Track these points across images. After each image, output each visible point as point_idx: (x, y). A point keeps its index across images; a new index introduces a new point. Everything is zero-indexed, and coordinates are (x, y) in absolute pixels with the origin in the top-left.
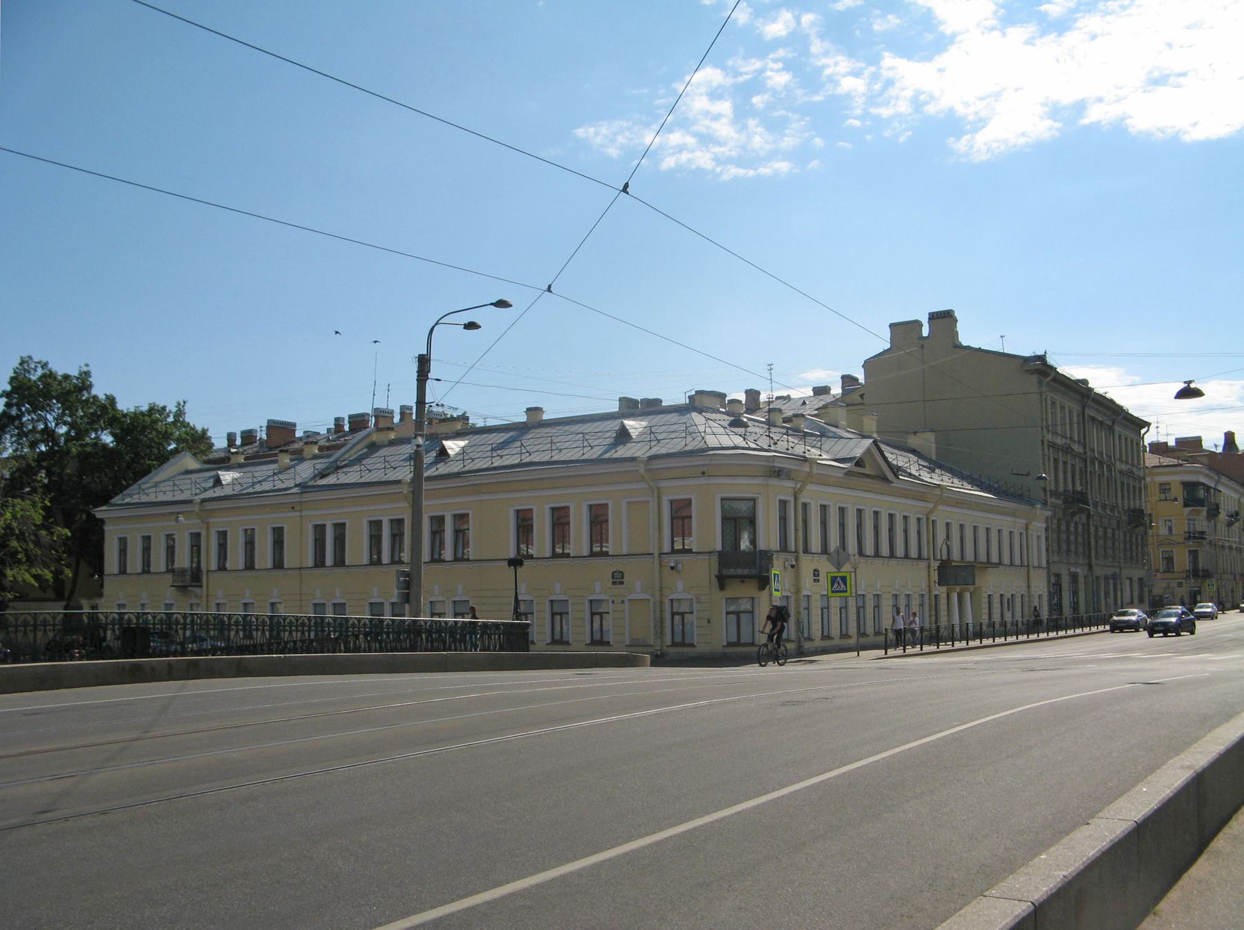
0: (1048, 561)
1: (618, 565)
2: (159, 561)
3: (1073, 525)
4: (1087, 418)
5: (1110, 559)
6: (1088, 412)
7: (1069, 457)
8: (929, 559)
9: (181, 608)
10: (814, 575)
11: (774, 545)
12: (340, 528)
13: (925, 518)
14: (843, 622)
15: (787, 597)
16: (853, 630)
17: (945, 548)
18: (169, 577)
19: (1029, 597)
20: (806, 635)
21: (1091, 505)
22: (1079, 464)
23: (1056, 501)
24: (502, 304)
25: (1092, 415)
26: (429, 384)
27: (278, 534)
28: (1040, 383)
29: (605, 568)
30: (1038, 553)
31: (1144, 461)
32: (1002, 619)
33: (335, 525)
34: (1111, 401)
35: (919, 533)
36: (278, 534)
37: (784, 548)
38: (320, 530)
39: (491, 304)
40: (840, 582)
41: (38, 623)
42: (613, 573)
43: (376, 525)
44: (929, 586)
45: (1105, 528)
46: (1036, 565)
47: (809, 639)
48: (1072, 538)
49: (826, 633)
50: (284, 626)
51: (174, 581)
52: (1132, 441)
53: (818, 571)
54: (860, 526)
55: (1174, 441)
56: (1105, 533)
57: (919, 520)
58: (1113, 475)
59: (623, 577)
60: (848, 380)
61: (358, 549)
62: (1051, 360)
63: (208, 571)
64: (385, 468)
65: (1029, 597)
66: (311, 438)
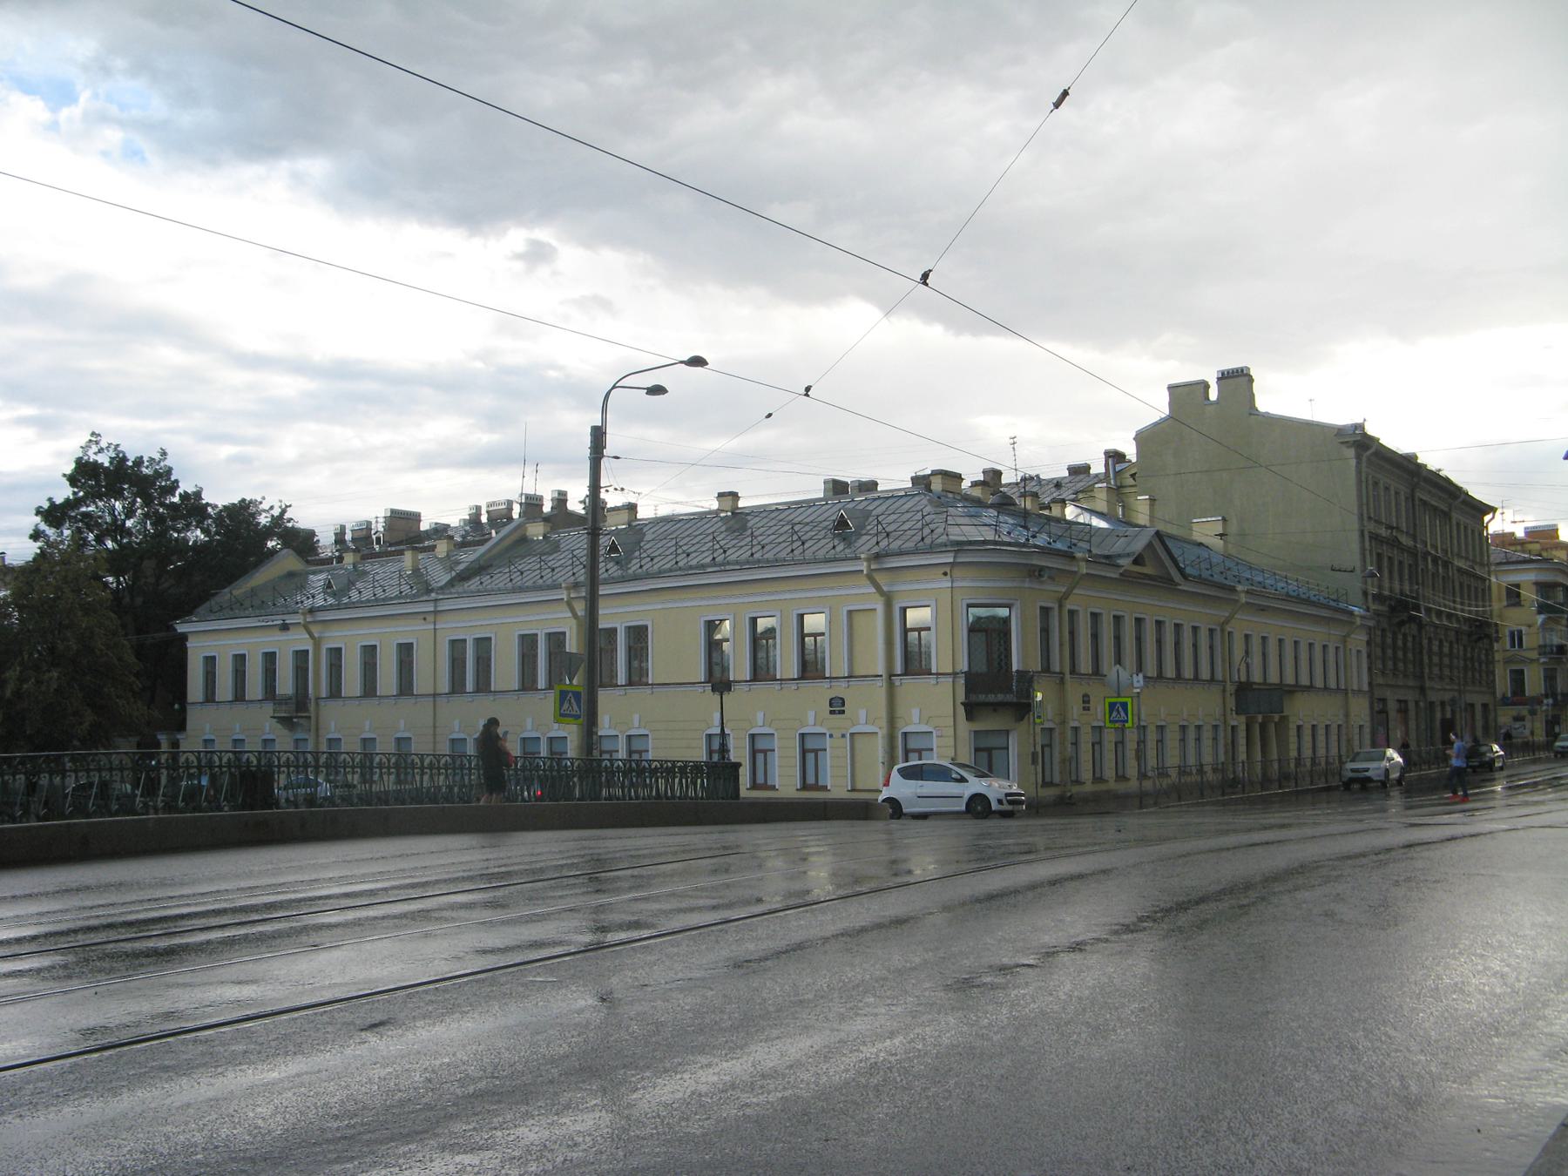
0: (1370, 684)
1: (839, 690)
2: (254, 687)
3: (1400, 637)
4: (1417, 502)
5: (1447, 680)
6: (1419, 494)
7: (1395, 552)
8: (1224, 681)
9: (284, 741)
10: (1084, 702)
11: (1035, 665)
12: (483, 644)
13: (1218, 629)
14: (1096, 762)
15: (1051, 730)
16: (1109, 773)
17: (1243, 665)
18: (269, 708)
19: (1347, 728)
20: (1074, 778)
21: (1423, 611)
22: (1407, 560)
23: (1380, 608)
24: (697, 362)
25: (1424, 498)
26: (604, 463)
27: (406, 651)
28: (1358, 457)
29: (820, 692)
30: (1359, 677)
31: (1488, 557)
32: (1299, 755)
33: (478, 641)
34: (1447, 480)
35: (1211, 647)
36: (406, 651)
37: (1047, 669)
38: (457, 646)
39: (682, 362)
40: (573, 700)
41: (321, 763)
42: (831, 700)
43: (528, 642)
44: (1224, 715)
45: (1441, 641)
46: (1355, 688)
47: (1078, 782)
48: (1400, 654)
49: (1098, 775)
50: (439, 768)
51: (274, 711)
52: (1466, 528)
53: (1088, 696)
54: (1177, 644)
55: (1523, 530)
56: (1441, 646)
57: (1211, 631)
58: (1450, 574)
59: (843, 705)
60: (1115, 457)
61: (506, 671)
62: (1371, 430)
63: (318, 699)
64: (540, 568)
65: (1347, 728)
66: (441, 531)
